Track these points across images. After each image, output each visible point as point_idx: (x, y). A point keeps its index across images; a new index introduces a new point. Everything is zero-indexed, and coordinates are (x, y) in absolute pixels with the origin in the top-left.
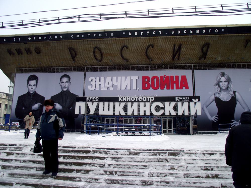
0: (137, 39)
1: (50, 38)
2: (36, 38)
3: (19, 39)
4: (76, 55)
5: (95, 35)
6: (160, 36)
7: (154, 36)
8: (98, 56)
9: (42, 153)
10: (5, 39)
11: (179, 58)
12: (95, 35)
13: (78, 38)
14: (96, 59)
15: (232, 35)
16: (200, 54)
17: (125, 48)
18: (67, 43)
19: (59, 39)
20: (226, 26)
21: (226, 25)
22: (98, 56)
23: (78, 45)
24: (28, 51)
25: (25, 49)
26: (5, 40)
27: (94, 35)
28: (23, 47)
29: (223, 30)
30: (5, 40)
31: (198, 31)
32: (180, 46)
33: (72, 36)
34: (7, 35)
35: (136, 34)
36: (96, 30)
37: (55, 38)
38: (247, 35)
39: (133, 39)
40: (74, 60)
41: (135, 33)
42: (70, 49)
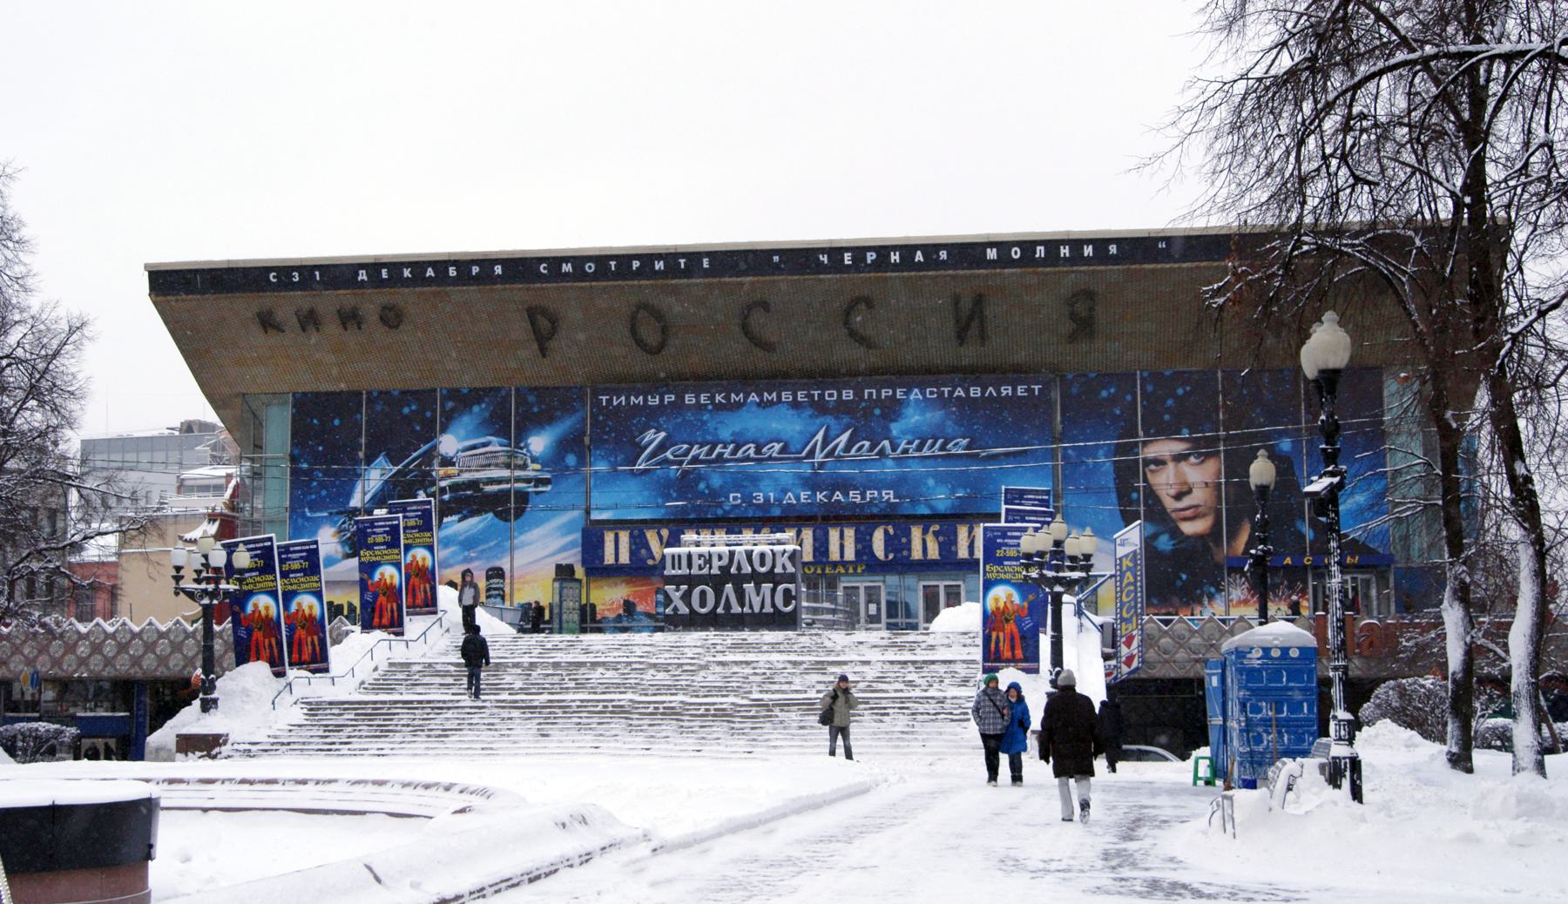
0: (505, 289)
1: (430, 272)
2: (710, 263)
3: (317, 273)
4: (554, 330)
5: (636, 264)
6: (680, 278)
7: (1013, 263)
8: (650, 335)
9: (1530, 486)
10: (545, 265)
11: (983, 337)
12: (636, 264)
13: (567, 274)
14: (640, 342)
15: (1170, 268)
16: (1067, 327)
17: (863, 306)
18: (519, 293)
19: (579, 274)
20: (1147, 235)
21: (229, 261)
22: (650, 335)
23: (567, 301)
24: (350, 318)
25: (339, 311)
26: (274, 277)
27: (634, 262)
28: (329, 301)
29: (776, 259)
30: (274, 277)
31: (1065, 251)
32: (979, 300)
33: (542, 267)
34: (196, 263)
35: (452, 272)
36: (326, 258)
37: (1037, 256)
38: (1179, 268)
39: (492, 290)
40: (543, 351)
41: (451, 272)
42: (532, 313)
